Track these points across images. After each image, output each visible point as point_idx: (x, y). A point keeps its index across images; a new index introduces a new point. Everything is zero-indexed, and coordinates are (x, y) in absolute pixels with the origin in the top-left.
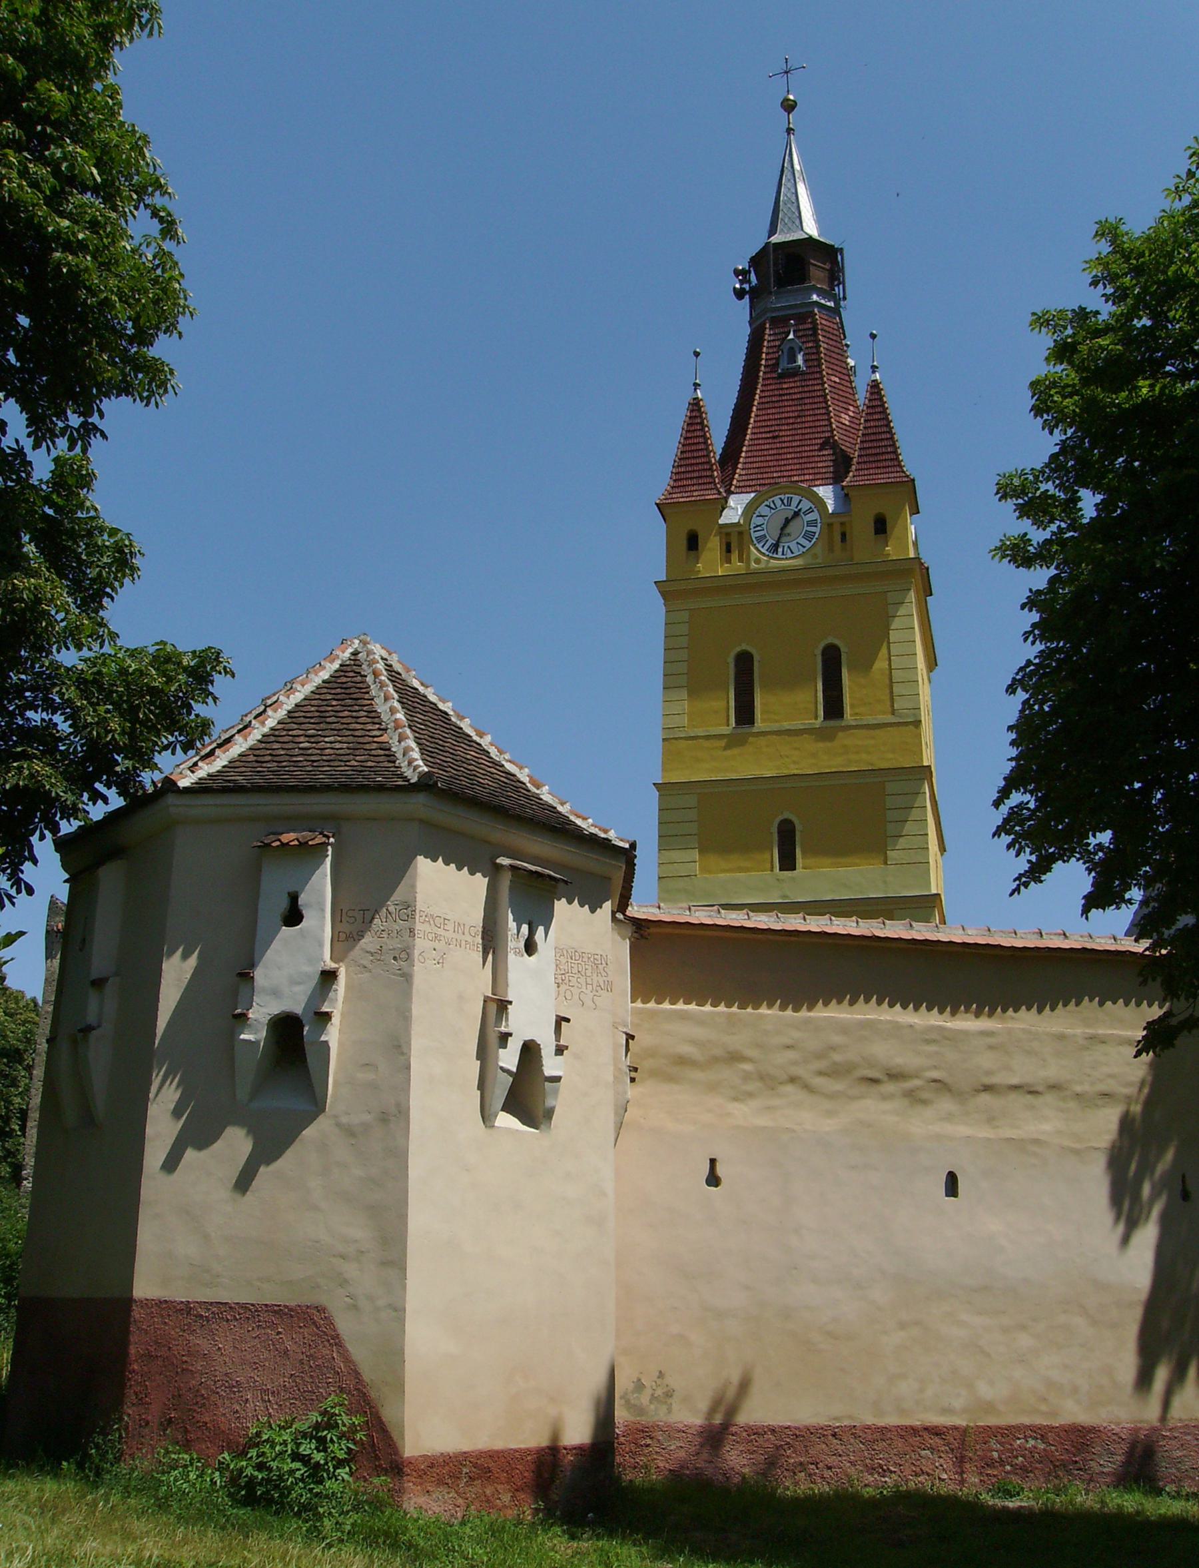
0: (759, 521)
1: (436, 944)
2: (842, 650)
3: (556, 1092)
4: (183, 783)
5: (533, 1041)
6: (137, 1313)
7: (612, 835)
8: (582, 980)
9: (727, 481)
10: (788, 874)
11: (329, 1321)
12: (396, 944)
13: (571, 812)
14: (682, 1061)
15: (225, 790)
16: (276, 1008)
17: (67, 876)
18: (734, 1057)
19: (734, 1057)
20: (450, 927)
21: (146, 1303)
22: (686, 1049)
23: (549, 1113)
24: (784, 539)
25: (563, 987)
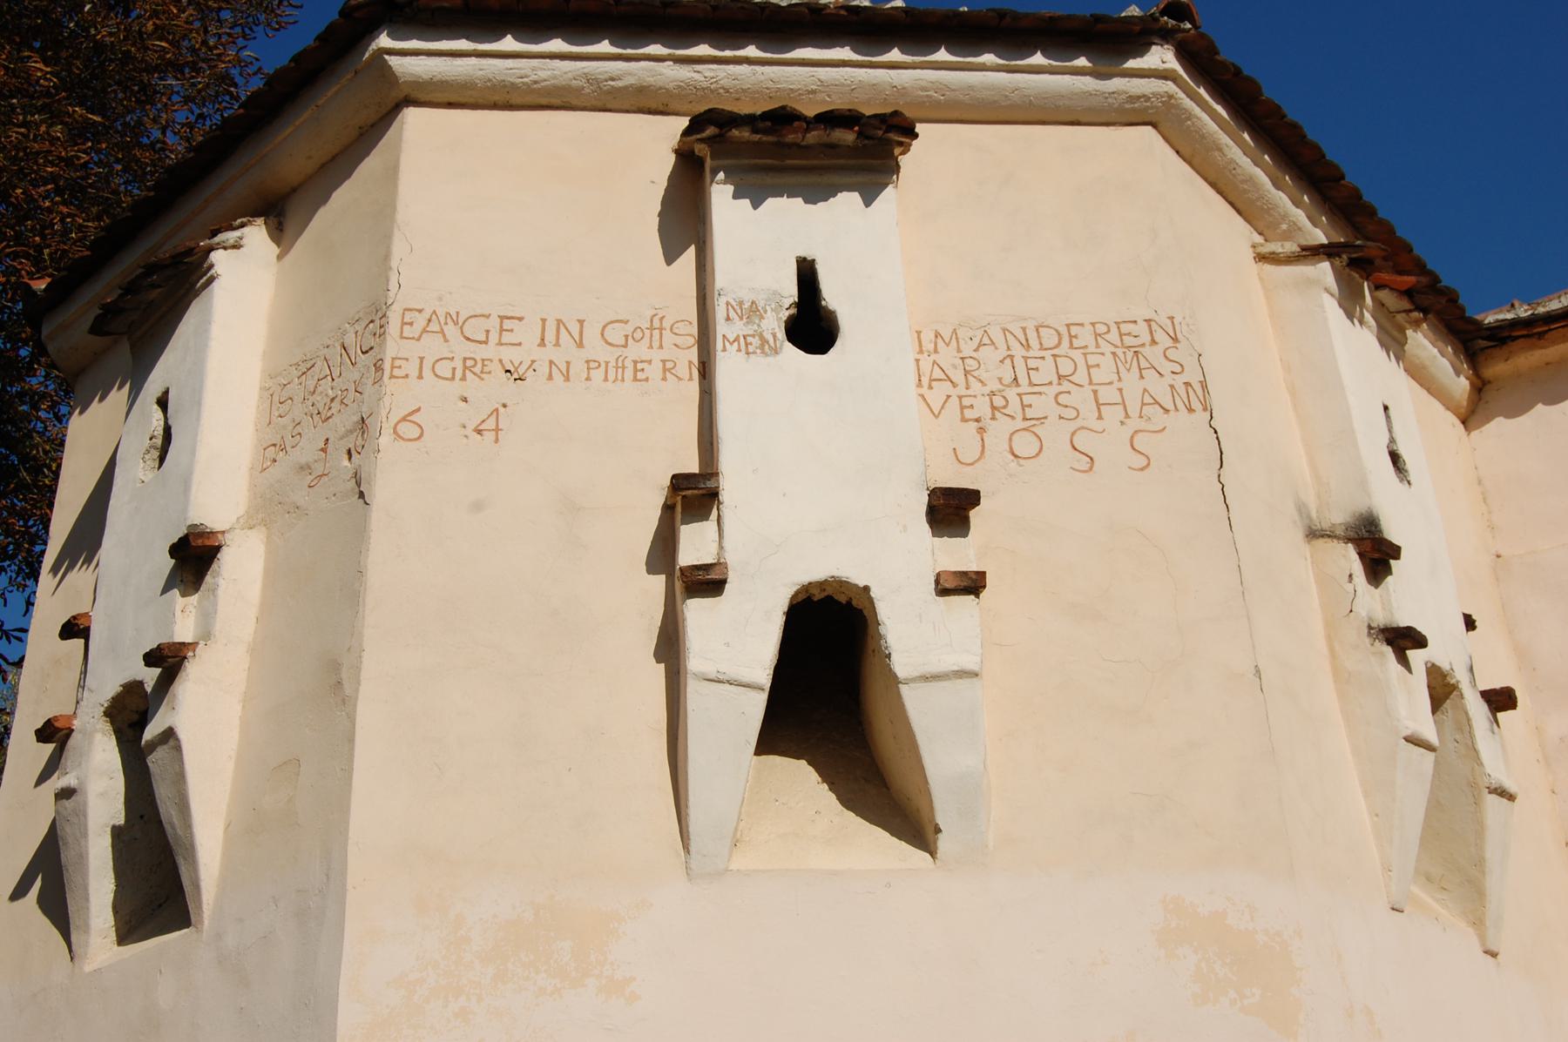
8: (1080, 398)
20: (526, 334)
25: (999, 429)
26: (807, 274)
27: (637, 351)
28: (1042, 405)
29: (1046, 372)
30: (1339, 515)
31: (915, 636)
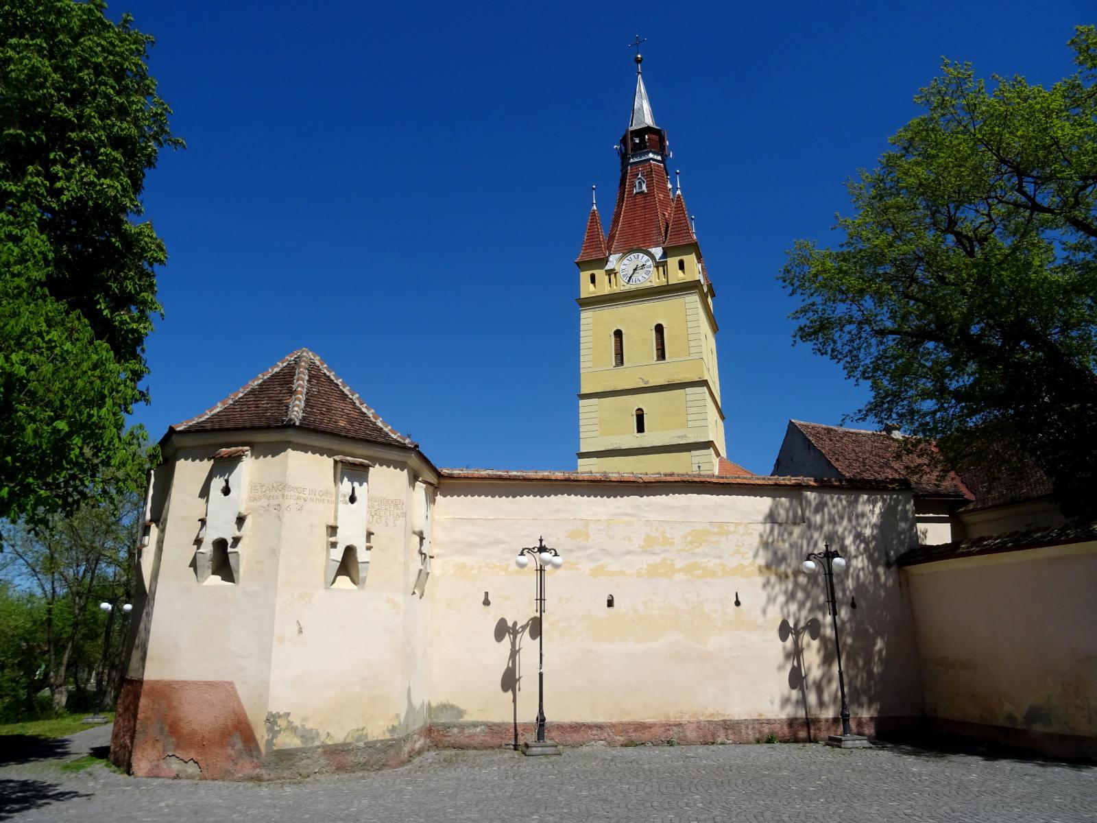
0: (624, 267)
1: (298, 501)
2: (107, 405)
3: (366, 569)
4: (178, 429)
5: (355, 548)
6: (145, 687)
7: (407, 441)
8: (388, 513)
9: (609, 248)
10: (640, 434)
11: (234, 688)
12: (276, 502)
13: (390, 430)
14: (471, 545)
15: (198, 431)
16: (216, 536)
17: (270, 456)
18: (498, 542)
19: (498, 542)
20: (307, 492)
21: (147, 681)
22: (473, 539)
23: (364, 579)
24: (635, 275)
25: (375, 517)
26: (487, 594)
27: (323, 497)
28: (382, 514)
29: (384, 508)
30: (417, 530)
31: (362, 555)
